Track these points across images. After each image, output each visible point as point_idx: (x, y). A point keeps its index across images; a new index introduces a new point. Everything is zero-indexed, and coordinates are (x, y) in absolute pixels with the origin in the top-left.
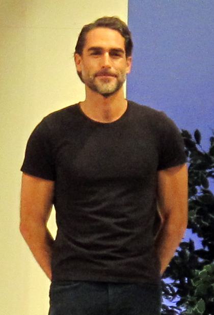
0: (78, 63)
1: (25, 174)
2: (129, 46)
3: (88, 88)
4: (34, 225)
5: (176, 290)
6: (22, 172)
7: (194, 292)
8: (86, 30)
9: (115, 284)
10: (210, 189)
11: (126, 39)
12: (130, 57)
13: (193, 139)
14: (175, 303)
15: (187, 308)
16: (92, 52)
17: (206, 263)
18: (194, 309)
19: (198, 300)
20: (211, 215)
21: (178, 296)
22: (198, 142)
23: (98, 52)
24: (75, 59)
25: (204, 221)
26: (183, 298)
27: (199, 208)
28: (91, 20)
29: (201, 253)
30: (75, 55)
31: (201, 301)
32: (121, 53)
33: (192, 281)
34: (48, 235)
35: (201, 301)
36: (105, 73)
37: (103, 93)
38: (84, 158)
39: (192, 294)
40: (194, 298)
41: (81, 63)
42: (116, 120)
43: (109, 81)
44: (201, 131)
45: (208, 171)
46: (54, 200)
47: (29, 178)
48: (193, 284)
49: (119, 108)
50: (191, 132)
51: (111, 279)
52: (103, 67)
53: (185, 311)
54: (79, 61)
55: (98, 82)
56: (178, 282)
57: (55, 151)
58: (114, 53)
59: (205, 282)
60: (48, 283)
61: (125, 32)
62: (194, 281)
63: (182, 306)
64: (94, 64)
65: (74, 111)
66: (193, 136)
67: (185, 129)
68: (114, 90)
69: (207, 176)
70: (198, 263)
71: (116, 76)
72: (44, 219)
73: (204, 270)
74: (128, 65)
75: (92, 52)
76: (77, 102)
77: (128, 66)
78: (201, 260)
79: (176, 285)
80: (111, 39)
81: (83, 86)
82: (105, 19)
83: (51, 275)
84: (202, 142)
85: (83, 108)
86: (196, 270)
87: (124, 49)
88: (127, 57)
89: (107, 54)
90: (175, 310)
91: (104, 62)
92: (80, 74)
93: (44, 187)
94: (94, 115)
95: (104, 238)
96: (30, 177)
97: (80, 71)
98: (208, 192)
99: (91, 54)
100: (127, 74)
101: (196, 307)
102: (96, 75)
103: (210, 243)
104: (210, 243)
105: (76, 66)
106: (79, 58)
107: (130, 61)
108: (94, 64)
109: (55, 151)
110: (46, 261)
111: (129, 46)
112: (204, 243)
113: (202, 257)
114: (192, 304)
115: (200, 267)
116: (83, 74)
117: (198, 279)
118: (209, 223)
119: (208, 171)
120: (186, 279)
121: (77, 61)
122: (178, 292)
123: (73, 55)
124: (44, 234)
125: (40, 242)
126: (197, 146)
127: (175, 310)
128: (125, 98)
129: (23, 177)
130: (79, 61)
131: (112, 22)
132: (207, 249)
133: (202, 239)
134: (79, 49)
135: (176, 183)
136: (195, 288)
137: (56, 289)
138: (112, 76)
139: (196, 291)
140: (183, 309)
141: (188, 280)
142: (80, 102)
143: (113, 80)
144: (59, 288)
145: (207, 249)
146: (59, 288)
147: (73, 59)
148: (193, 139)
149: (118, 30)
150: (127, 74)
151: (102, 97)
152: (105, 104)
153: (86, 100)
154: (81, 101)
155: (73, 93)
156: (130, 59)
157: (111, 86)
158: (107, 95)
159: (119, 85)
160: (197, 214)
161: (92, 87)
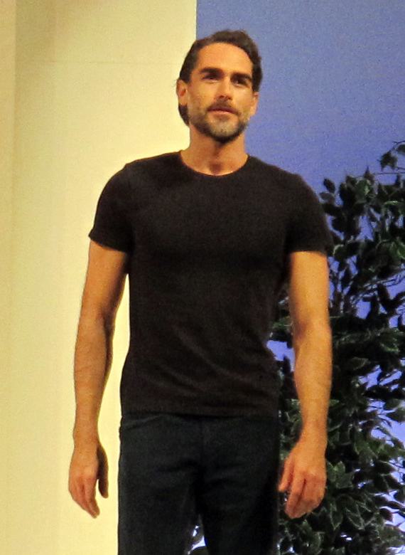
0: (180, 93)
1: (93, 242)
2: (256, 78)
7: (290, 430)
9: (210, 418)
16: (205, 74)
20: (277, 349)
23: (214, 74)
24: (178, 88)
33: (287, 414)
36: (222, 105)
37: (217, 134)
43: (227, 119)
47: (97, 247)
49: (235, 158)
51: (208, 410)
52: (222, 97)
55: (211, 119)
57: (138, 213)
58: (238, 78)
64: (208, 92)
65: (170, 162)
68: (235, 131)
75: (205, 74)
76: (177, 150)
80: (232, 59)
86: (293, 400)
89: (227, 79)
92: (183, 111)
96: (99, 247)
99: (204, 78)
102: (210, 109)
107: (257, 98)
108: (208, 92)
109: (138, 213)
116: (190, 108)
120: (280, 412)
123: (176, 82)
134: (185, 75)
135: (312, 275)
137: (127, 424)
144: (134, 422)
146: (134, 422)
147: (175, 88)
149: (244, 48)
152: (216, 154)
155: (175, 138)
156: (257, 96)
157: (229, 126)
159: (241, 127)
161: (201, 128)
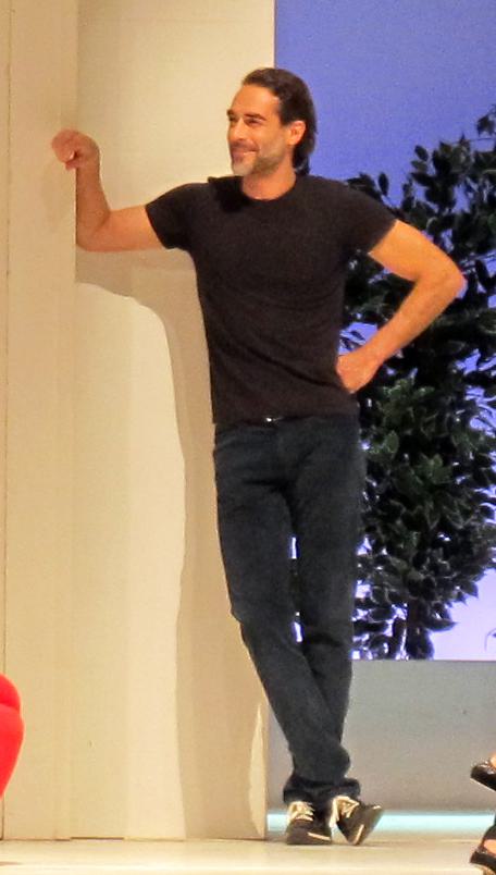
13: (378, 188)
16: (248, 118)
17: (398, 377)
19: (387, 433)
22: (385, 193)
27: (386, 292)
31: (393, 434)
33: (378, 403)
35: (393, 434)
39: (378, 423)
44: (388, 175)
50: (374, 177)
60: (238, 625)
66: (377, 182)
67: (364, 172)
73: (397, 387)
84: (389, 192)
86: (385, 388)
101: (384, 444)
114: (378, 439)
120: (370, 401)
126: (383, 197)
128: (415, 544)
133: (400, 355)
137: (224, 443)
141: (373, 403)
142: (229, 138)
148: (378, 188)
160: (385, 302)
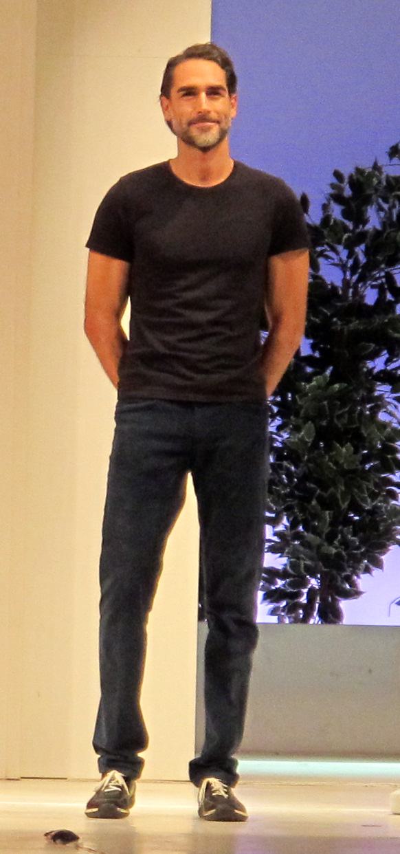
0: (165, 109)
3: (180, 139)
4: (103, 320)
5: (275, 409)
6: (88, 250)
8: (171, 65)
9: (202, 405)
10: (321, 273)
11: (227, 71)
12: (234, 96)
14: (275, 427)
15: (290, 434)
16: (182, 93)
17: (314, 374)
18: (300, 436)
19: (305, 423)
21: (278, 418)
23: (190, 92)
24: (162, 104)
25: (314, 317)
26: (285, 420)
28: (179, 50)
29: (309, 360)
30: (160, 99)
31: (310, 425)
32: (221, 91)
33: (297, 397)
34: (120, 332)
36: (203, 118)
37: (200, 145)
38: (171, 233)
39: (297, 415)
40: (300, 421)
41: (170, 108)
42: (213, 185)
43: (209, 128)
44: (310, 197)
45: (319, 249)
46: (129, 289)
47: (100, 258)
48: (300, 403)
51: (200, 398)
52: (200, 112)
53: (289, 438)
54: (167, 107)
55: (194, 131)
56: (279, 399)
57: (132, 222)
58: (213, 92)
59: (314, 399)
61: (225, 64)
62: (300, 398)
63: (285, 432)
64: (187, 108)
65: (162, 172)
68: (216, 141)
69: (318, 256)
70: (306, 373)
71: (218, 122)
72: (118, 314)
73: (314, 383)
74: (233, 105)
75: (182, 93)
76: (166, 160)
77: (233, 107)
78: (309, 370)
79: (276, 404)
80: (208, 73)
81: (173, 139)
82: (196, 47)
83: (117, 380)
85: (175, 170)
86: (303, 384)
87: (225, 86)
88: (230, 96)
89: (203, 95)
90: (274, 436)
91: (201, 105)
92: (169, 124)
93: (117, 268)
94: (191, 179)
95: (190, 340)
97: (169, 119)
98: (320, 278)
99: (184, 95)
100: (232, 119)
101: (303, 433)
102: (190, 124)
103: (322, 346)
104: (322, 346)
105: (164, 113)
106: (166, 102)
108: (187, 108)
109: (132, 222)
110: (114, 364)
111: (232, 81)
112: (314, 347)
113: (311, 366)
114: (297, 429)
115: (308, 379)
116: (174, 122)
117: (306, 395)
118: (321, 320)
119: (319, 249)
120: (290, 395)
121: (165, 106)
122: (278, 413)
123: (158, 98)
124: (114, 333)
125: (107, 336)
127: (274, 436)
129: (89, 254)
130: (167, 107)
131: (207, 50)
132: (317, 355)
134: (166, 90)
136: (301, 407)
138: (214, 122)
139: (302, 412)
140: (286, 436)
141: (293, 397)
142: (170, 160)
143: (214, 128)
145: (317, 355)
147: (159, 103)
149: (215, 60)
150: (232, 119)
151: (200, 152)
152: (204, 160)
153: (178, 155)
154: (171, 158)
155: (162, 148)
157: (211, 136)
158: (205, 149)
161: (186, 140)
